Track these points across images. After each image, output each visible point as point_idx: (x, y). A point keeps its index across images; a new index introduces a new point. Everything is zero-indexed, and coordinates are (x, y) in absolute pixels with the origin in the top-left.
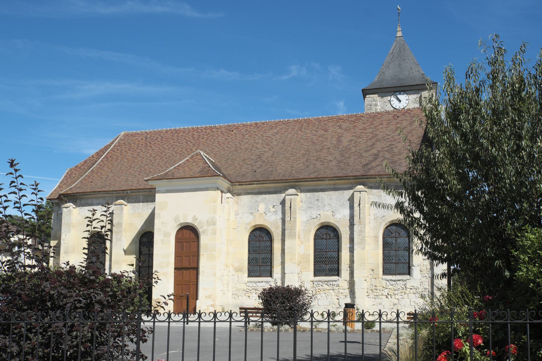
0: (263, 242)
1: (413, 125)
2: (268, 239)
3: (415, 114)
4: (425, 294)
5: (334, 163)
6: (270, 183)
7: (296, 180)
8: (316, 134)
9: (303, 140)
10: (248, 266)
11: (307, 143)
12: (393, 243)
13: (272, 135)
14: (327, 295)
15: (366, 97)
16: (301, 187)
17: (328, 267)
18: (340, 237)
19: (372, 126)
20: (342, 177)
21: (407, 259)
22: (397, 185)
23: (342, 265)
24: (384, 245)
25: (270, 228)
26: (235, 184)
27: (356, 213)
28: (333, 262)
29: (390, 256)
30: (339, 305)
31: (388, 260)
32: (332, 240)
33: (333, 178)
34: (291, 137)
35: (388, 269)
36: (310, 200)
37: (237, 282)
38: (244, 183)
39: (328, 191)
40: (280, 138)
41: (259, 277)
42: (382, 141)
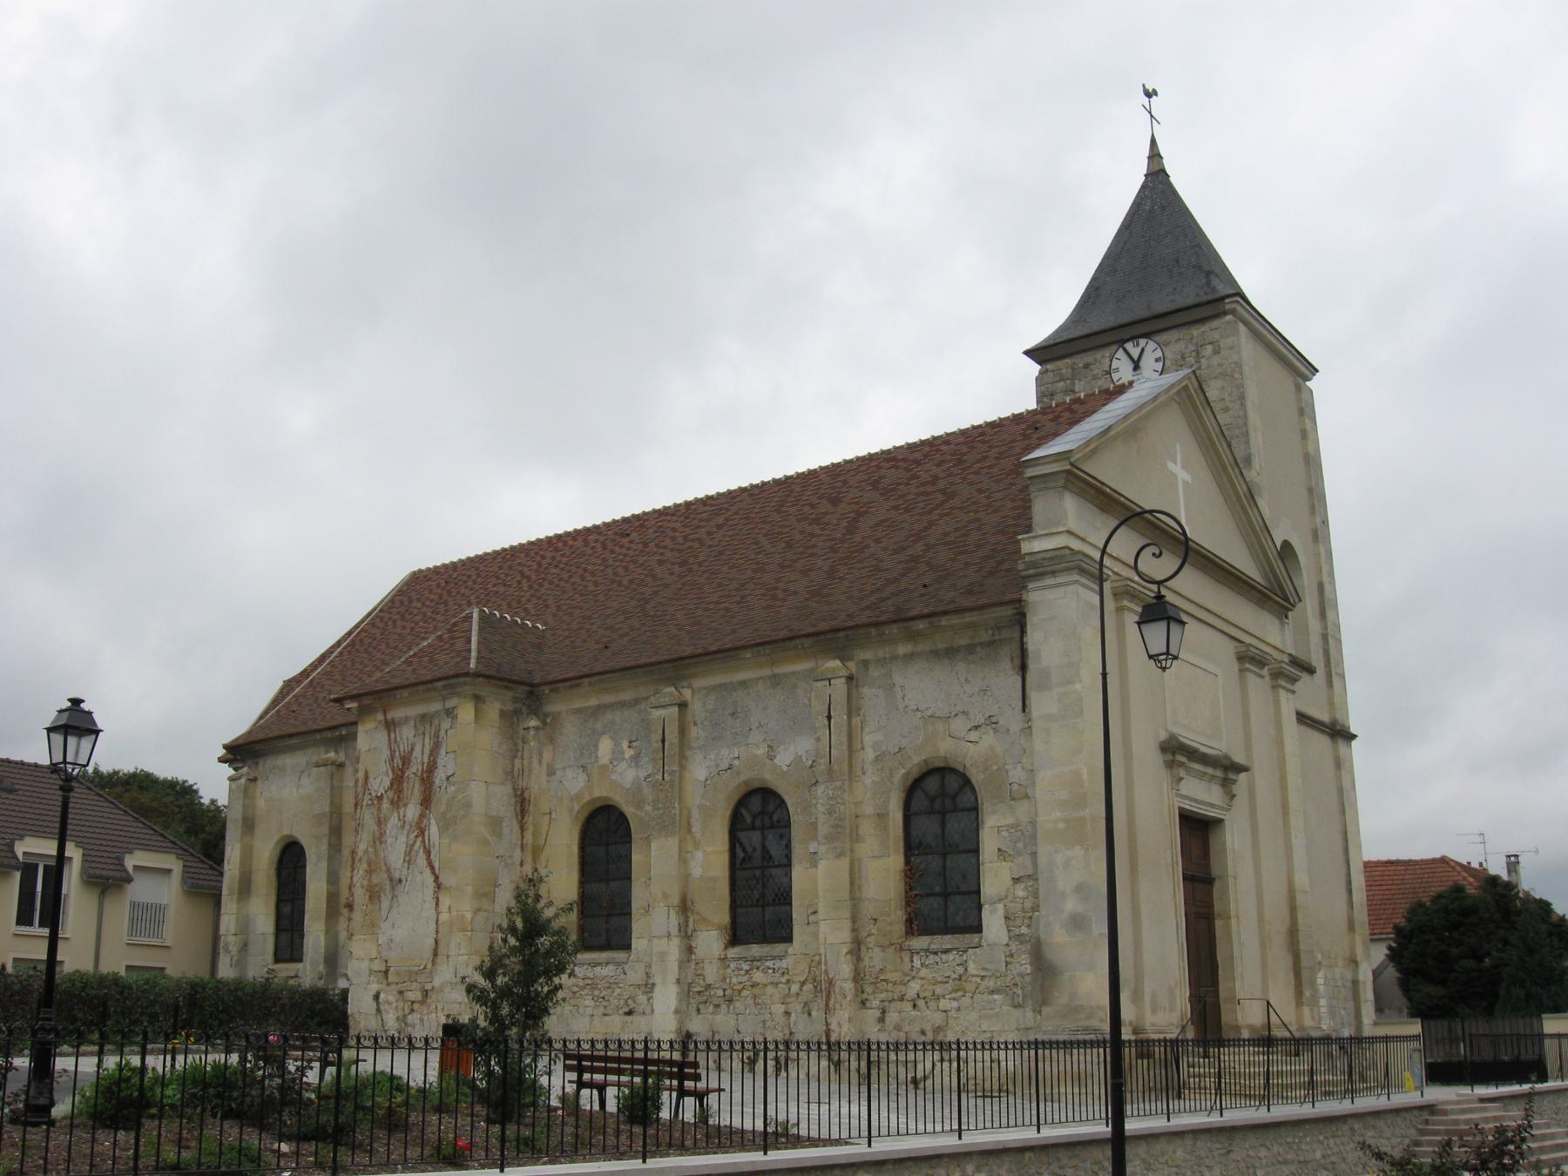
22: (933, 648)
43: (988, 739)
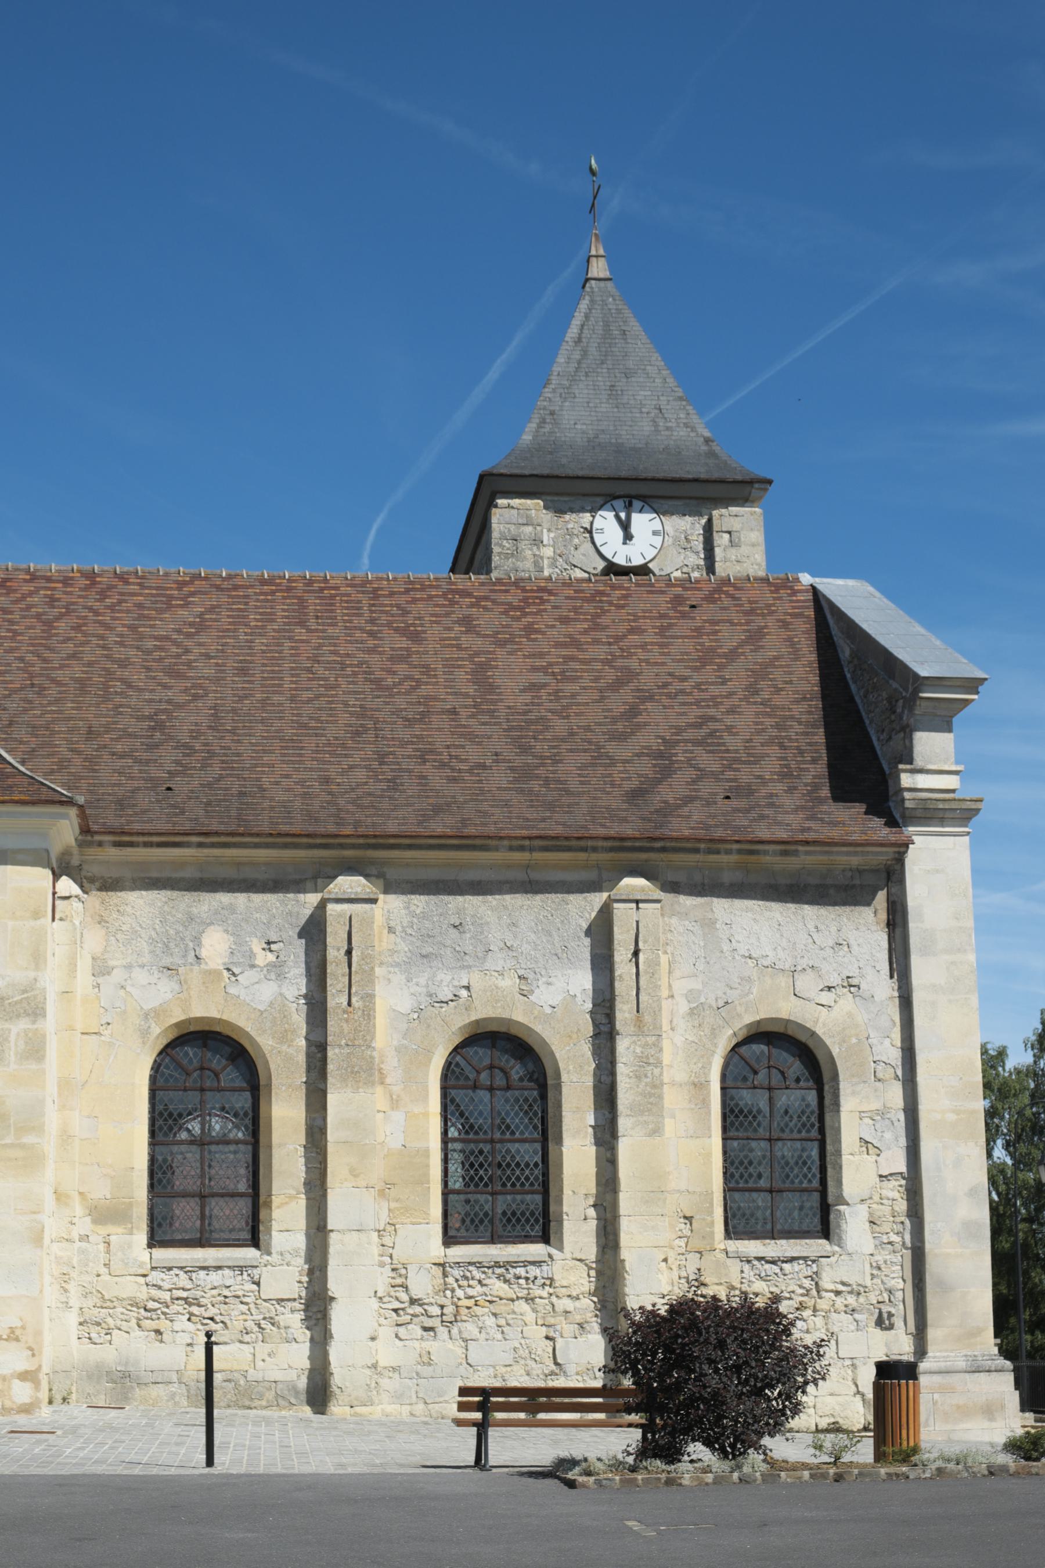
0: (218, 1095)
1: (762, 647)
2: (240, 1083)
3: (756, 602)
4: (893, 1311)
5: (499, 778)
6: (257, 846)
7: (373, 841)
8: (376, 646)
9: (326, 669)
10: (150, 1200)
11: (350, 683)
12: (759, 1111)
13: (179, 631)
14: (502, 1322)
15: (496, 506)
16: (385, 870)
17: (503, 1203)
18: (550, 1082)
19: (602, 636)
20: (567, 838)
21: (814, 1176)
23: (565, 1197)
24: (724, 1117)
25: (253, 1033)
26: (97, 838)
27: (624, 987)
28: (523, 1185)
29: (751, 1163)
30: (556, 1364)
31: (742, 1176)
32: (517, 1093)
33: (527, 843)
34: (271, 651)
35: (744, 1215)
36: (427, 924)
37: (103, 1270)
38: (141, 839)
39: (500, 892)
40: (222, 651)
41: (202, 1246)
42: (666, 701)
43: (846, 1003)
